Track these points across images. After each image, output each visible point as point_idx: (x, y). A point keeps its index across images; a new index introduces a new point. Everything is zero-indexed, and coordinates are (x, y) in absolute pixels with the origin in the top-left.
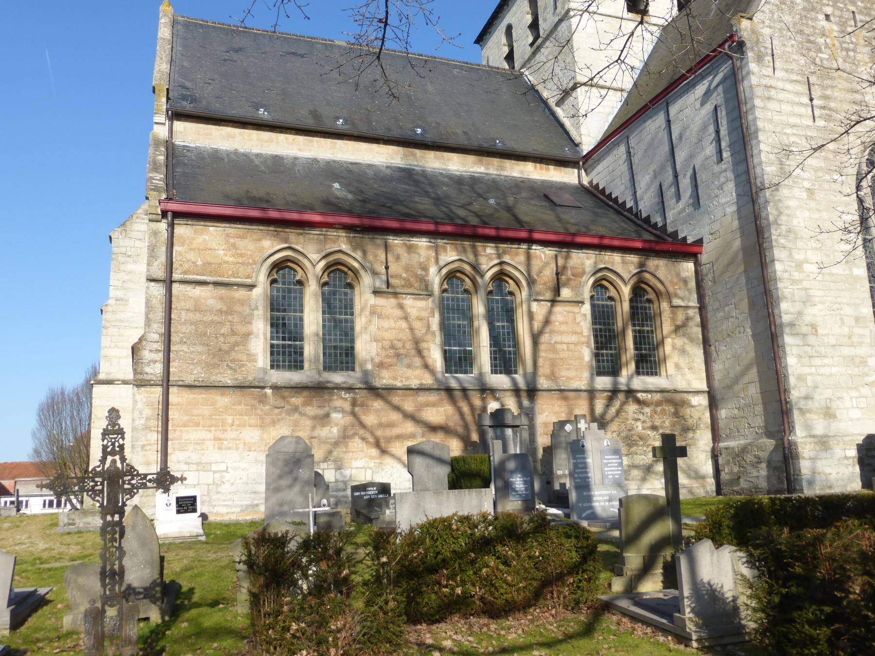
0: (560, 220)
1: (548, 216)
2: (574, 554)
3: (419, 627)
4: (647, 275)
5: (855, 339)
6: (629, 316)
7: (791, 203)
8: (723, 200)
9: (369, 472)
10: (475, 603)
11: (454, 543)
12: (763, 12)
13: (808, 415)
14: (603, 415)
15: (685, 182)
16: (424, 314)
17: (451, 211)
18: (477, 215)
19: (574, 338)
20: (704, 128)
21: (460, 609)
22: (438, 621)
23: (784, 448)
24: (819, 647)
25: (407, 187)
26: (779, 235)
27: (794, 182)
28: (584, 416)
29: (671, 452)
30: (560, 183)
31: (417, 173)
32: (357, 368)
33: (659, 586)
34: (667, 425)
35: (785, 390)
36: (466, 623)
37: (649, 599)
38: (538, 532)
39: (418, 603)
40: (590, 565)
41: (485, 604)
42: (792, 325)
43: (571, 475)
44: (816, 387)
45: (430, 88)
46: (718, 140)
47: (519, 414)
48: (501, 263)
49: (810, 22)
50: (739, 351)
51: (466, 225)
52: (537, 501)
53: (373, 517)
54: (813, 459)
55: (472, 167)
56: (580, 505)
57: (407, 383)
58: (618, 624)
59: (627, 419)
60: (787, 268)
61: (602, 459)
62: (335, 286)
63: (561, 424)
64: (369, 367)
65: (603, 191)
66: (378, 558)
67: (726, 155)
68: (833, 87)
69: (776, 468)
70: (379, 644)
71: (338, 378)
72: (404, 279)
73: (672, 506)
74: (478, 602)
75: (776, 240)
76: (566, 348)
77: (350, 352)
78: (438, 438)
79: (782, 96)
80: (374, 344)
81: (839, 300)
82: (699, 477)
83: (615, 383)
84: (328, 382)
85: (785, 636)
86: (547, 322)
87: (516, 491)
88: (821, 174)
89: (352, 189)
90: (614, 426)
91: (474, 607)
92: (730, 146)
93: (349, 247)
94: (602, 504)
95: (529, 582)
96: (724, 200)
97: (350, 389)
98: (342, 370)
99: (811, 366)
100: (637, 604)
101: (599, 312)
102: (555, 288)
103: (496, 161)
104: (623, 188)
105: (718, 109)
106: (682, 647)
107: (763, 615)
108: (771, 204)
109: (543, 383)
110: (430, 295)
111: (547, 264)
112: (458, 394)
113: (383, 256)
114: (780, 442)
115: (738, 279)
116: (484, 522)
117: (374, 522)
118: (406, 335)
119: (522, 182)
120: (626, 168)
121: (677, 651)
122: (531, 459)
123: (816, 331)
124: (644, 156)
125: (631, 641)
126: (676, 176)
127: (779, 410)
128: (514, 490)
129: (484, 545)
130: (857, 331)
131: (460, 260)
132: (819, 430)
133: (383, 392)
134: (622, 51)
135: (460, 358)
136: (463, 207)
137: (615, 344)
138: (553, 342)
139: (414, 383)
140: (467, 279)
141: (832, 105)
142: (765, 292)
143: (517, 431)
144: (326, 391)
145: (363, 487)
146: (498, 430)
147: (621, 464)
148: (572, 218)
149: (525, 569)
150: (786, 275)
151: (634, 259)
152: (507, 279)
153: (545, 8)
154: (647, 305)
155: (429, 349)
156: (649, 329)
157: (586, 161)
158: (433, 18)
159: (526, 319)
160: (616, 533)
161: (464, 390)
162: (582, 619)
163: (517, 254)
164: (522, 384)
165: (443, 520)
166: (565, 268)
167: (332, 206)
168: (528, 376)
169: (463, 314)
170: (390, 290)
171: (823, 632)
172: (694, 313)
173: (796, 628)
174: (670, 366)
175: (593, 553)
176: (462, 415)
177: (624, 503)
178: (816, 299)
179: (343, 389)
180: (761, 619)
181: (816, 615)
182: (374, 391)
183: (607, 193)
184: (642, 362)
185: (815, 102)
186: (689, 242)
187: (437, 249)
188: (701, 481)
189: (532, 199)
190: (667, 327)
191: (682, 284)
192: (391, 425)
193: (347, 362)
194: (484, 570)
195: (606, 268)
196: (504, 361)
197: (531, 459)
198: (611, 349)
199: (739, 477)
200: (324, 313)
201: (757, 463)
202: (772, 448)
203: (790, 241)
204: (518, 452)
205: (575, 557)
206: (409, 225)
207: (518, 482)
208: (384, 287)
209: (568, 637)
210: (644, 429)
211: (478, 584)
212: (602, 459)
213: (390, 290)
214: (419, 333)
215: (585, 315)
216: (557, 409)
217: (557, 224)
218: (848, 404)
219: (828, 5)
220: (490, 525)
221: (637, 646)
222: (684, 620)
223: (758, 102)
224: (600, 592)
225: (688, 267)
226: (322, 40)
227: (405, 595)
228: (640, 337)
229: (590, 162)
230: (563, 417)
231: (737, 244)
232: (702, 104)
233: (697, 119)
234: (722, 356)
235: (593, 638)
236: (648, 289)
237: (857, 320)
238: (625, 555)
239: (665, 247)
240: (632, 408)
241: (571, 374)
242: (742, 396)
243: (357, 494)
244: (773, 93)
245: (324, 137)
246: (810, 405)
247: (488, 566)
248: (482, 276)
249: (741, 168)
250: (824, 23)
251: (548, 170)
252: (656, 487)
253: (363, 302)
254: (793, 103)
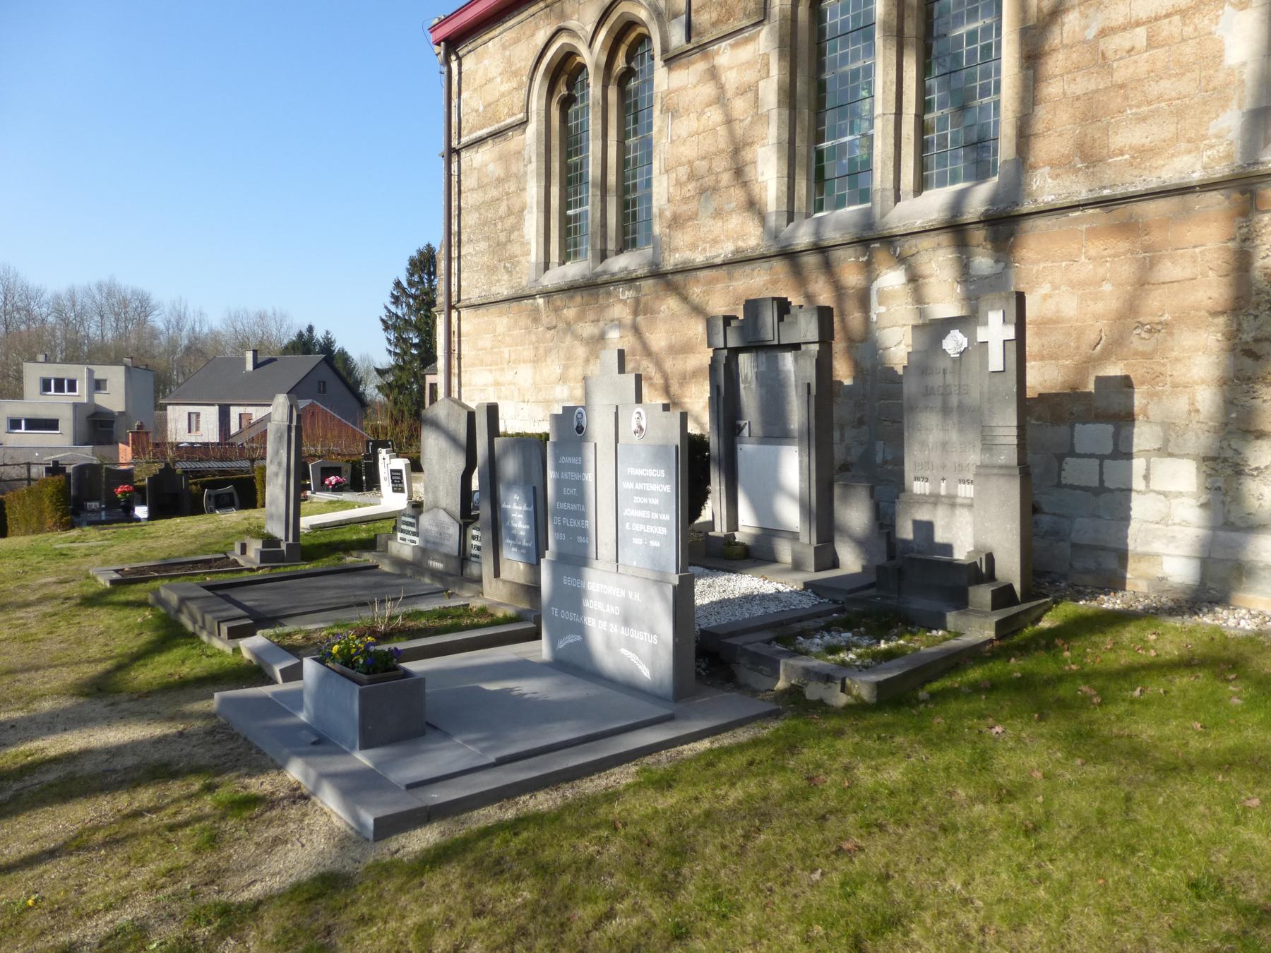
57: (711, 253)
71: (621, 263)
138: (1091, 34)
144: (602, 291)
161: (820, 249)
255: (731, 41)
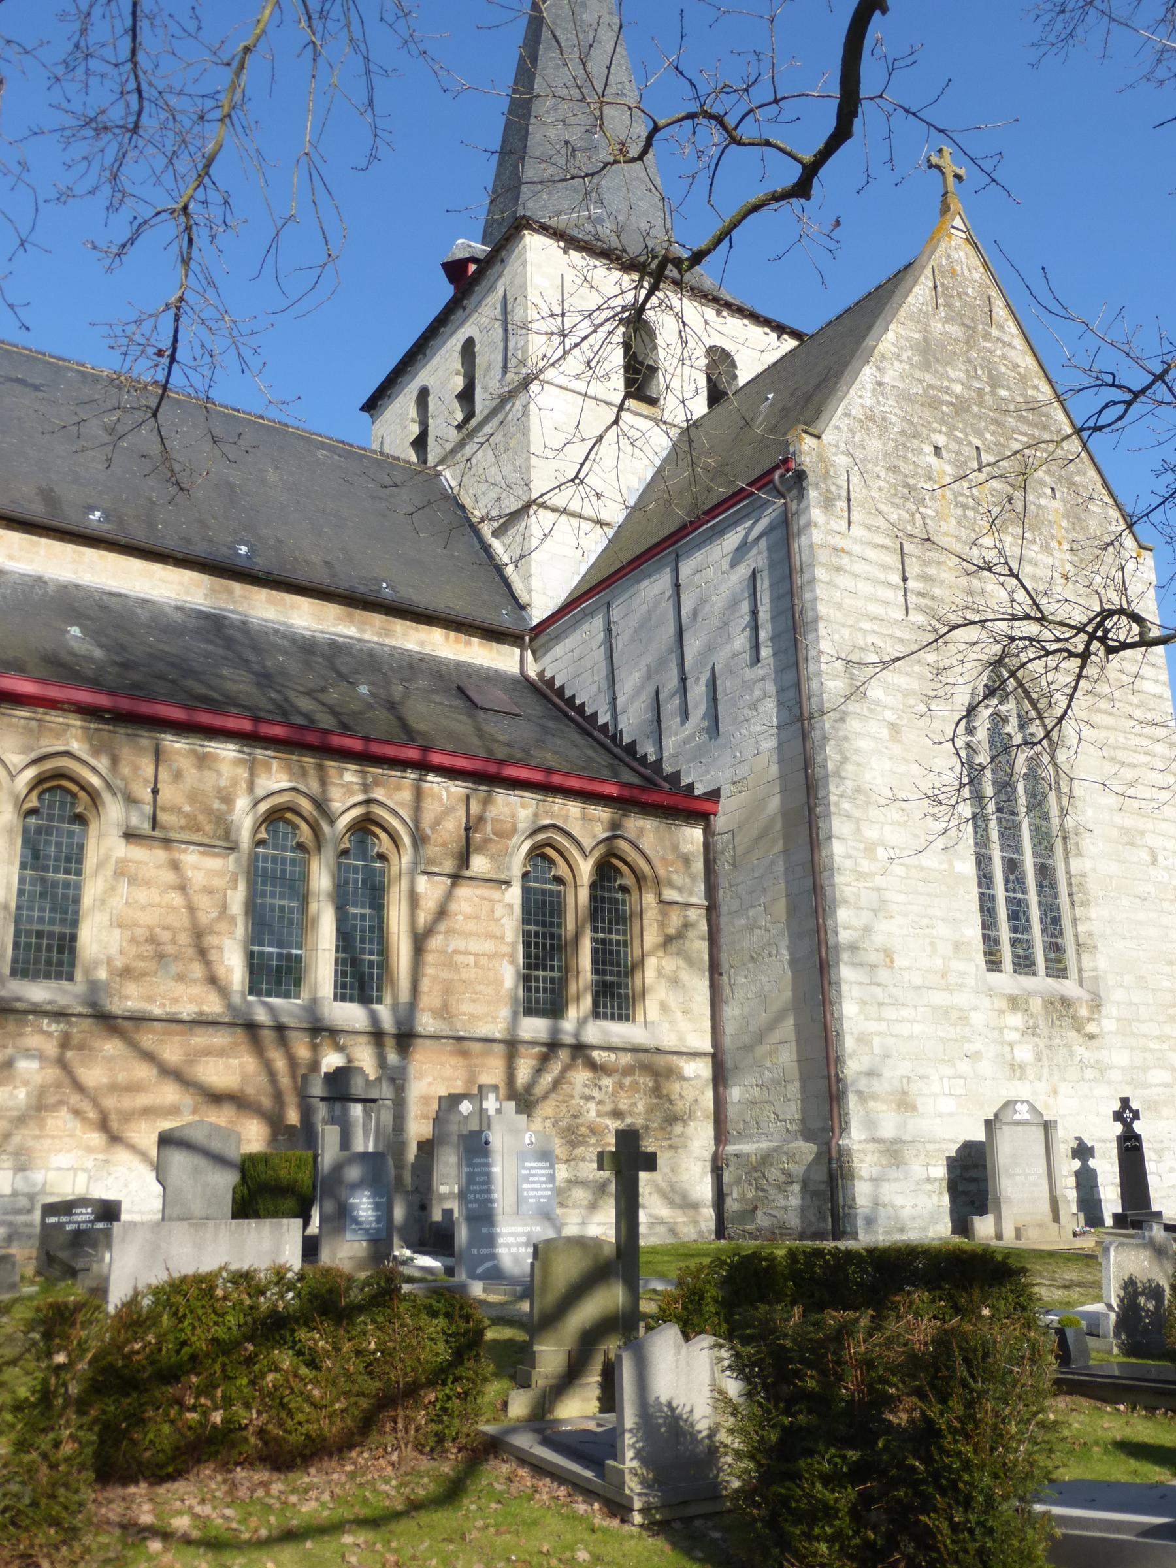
0: (480, 734)
1: (460, 724)
2: (441, 1347)
3: (132, 1489)
4: (623, 845)
5: (952, 979)
6: (587, 912)
7: (863, 744)
8: (757, 728)
9: (82, 1178)
10: (246, 1440)
11: (216, 1323)
12: (837, 428)
13: (872, 1104)
14: (529, 1088)
15: (698, 691)
16: (218, 883)
17: (286, 699)
18: (333, 711)
19: (488, 946)
20: (734, 604)
21: (217, 1452)
22: (171, 1478)
23: (830, 1159)
24: (837, 1522)
25: (210, 648)
26: (842, 796)
27: (870, 710)
28: (495, 1088)
29: (629, 1160)
30: (488, 669)
31: (233, 626)
32: (79, 976)
33: (593, 1406)
34: (637, 1108)
35: (837, 1059)
36: (225, 1481)
37: (571, 1432)
38: (378, 1305)
39: (134, 1443)
40: (467, 1369)
41: (266, 1443)
42: (853, 948)
43: (462, 1195)
44: (886, 1056)
45: (272, 476)
46: (755, 627)
47: (379, 1079)
48: (368, 802)
49: (910, 455)
50: (768, 987)
51: (310, 726)
52: (396, 1241)
53: (78, 1267)
54: (876, 1181)
55: (334, 625)
56: (474, 1251)
58: (510, 1480)
59: (572, 1097)
60: (851, 852)
61: (520, 1166)
62: (50, 818)
63: (453, 1101)
64: (102, 974)
65: (561, 691)
66: (49, 1355)
67: (765, 652)
68: (940, 563)
69: (815, 1194)
70: (33, 1529)
71: (38, 992)
72: (187, 816)
73: (624, 1260)
74: (252, 1440)
75: (837, 804)
76: (472, 963)
77: (67, 944)
78: (221, 1117)
79: (859, 567)
80: (117, 932)
81: (930, 911)
82: (689, 1205)
83: (555, 1031)
84: (18, 999)
85: (784, 1501)
86: (442, 913)
87: (358, 1223)
88: (912, 702)
89: (104, 640)
90: (546, 1109)
91: (244, 1448)
92: (772, 639)
93: (86, 747)
94: (514, 1250)
95: (353, 1400)
96: (757, 730)
97: (60, 1015)
98: (48, 976)
99: (880, 1019)
100: (547, 1442)
101: (536, 901)
102: (461, 854)
103: (378, 619)
104: (594, 689)
105: (758, 576)
106: (616, 1523)
107: (751, 1465)
108: (832, 742)
109: (426, 1023)
110: (233, 848)
111: (449, 811)
112: (268, 1036)
113: (149, 770)
114: (824, 1148)
115: (772, 863)
116: (277, 1283)
117: (81, 1276)
118: (181, 920)
119: (421, 660)
120: (603, 656)
121: (605, 1531)
122: (390, 1162)
123: (892, 961)
124: (632, 640)
125: (526, 1513)
126: (683, 679)
127: (825, 1094)
128: (355, 1221)
129: (273, 1328)
130: (956, 965)
131: (293, 789)
132: (887, 1131)
133: (126, 1023)
134: (582, 465)
135: (279, 968)
136: (308, 693)
137: (560, 960)
138: (450, 950)
139: (187, 1010)
140: (304, 826)
141: (937, 591)
142: (815, 889)
143: (371, 1110)
144: (12, 1017)
145: (67, 1207)
146: (338, 1106)
147: (552, 1178)
148: (502, 731)
149: (348, 1376)
150: (849, 864)
151: (602, 813)
152: (378, 831)
153: (488, 369)
154: (620, 896)
155: (220, 948)
156: (620, 937)
157: (537, 635)
158: (254, 362)
159: (405, 905)
160: (525, 1306)
161: (280, 1029)
162: (447, 1470)
163: (398, 788)
164: (387, 1021)
165: (198, 1279)
166: (481, 819)
167: (60, 667)
168: (401, 1008)
169: (292, 887)
170: (156, 833)
171: (843, 1498)
172: (697, 916)
173: (802, 1489)
174: (651, 1007)
175: (474, 1346)
176: (272, 1075)
177: (541, 1252)
178: (894, 907)
179: (46, 1014)
180: (746, 1471)
181: (836, 1465)
182: (106, 1021)
183: (568, 694)
184: (605, 996)
185: (911, 584)
186: (697, 792)
187: (253, 766)
188: (691, 1212)
189: (436, 692)
190: (651, 937)
191: (680, 865)
192: (133, 1088)
193: (60, 963)
194: (270, 1377)
195: (553, 826)
196: (361, 977)
197: (390, 1162)
198: (552, 969)
199: (756, 1208)
200: (23, 866)
201: (786, 1183)
202: (811, 1158)
203: (857, 807)
204: (371, 1149)
205: (443, 1351)
206: (204, 718)
207: (364, 1206)
208: (146, 827)
209: (415, 1506)
210: (599, 1115)
211: (255, 1405)
212: (520, 1166)
213: (156, 833)
214: (204, 918)
215: (510, 906)
216: (448, 1071)
217: (475, 741)
218: (936, 1088)
219: (940, 432)
220: (288, 1290)
221: (535, 1523)
222: (621, 1472)
223: (820, 573)
224: (484, 1419)
225: (693, 836)
226: (78, 364)
227: (96, 1429)
228: (604, 951)
229: (543, 638)
230: (458, 1088)
231: (775, 804)
232: (733, 565)
233: (722, 588)
234: (740, 994)
235: (460, 1508)
236: (624, 868)
237: (957, 946)
238: (537, 1348)
239: (655, 798)
240: (581, 1076)
241: (479, 1009)
242: (768, 1064)
243: (52, 1220)
244: (845, 561)
245: (62, 540)
246: (877, 1086)
247: (277, 1369)
248: (332, 822)
249: (789, 677)
250: (932, 459)
251: (468, 644)
252: (602, 1226)
253: (102, 851)
254: (876, 582)
255: (201, 849)
